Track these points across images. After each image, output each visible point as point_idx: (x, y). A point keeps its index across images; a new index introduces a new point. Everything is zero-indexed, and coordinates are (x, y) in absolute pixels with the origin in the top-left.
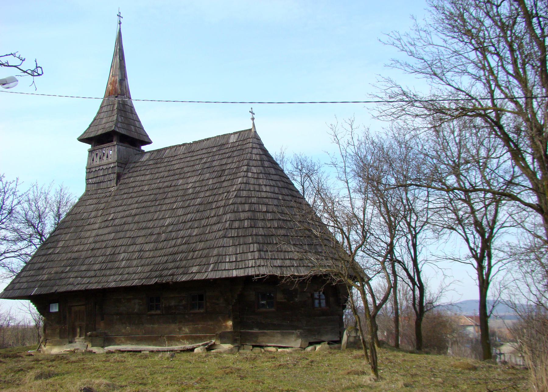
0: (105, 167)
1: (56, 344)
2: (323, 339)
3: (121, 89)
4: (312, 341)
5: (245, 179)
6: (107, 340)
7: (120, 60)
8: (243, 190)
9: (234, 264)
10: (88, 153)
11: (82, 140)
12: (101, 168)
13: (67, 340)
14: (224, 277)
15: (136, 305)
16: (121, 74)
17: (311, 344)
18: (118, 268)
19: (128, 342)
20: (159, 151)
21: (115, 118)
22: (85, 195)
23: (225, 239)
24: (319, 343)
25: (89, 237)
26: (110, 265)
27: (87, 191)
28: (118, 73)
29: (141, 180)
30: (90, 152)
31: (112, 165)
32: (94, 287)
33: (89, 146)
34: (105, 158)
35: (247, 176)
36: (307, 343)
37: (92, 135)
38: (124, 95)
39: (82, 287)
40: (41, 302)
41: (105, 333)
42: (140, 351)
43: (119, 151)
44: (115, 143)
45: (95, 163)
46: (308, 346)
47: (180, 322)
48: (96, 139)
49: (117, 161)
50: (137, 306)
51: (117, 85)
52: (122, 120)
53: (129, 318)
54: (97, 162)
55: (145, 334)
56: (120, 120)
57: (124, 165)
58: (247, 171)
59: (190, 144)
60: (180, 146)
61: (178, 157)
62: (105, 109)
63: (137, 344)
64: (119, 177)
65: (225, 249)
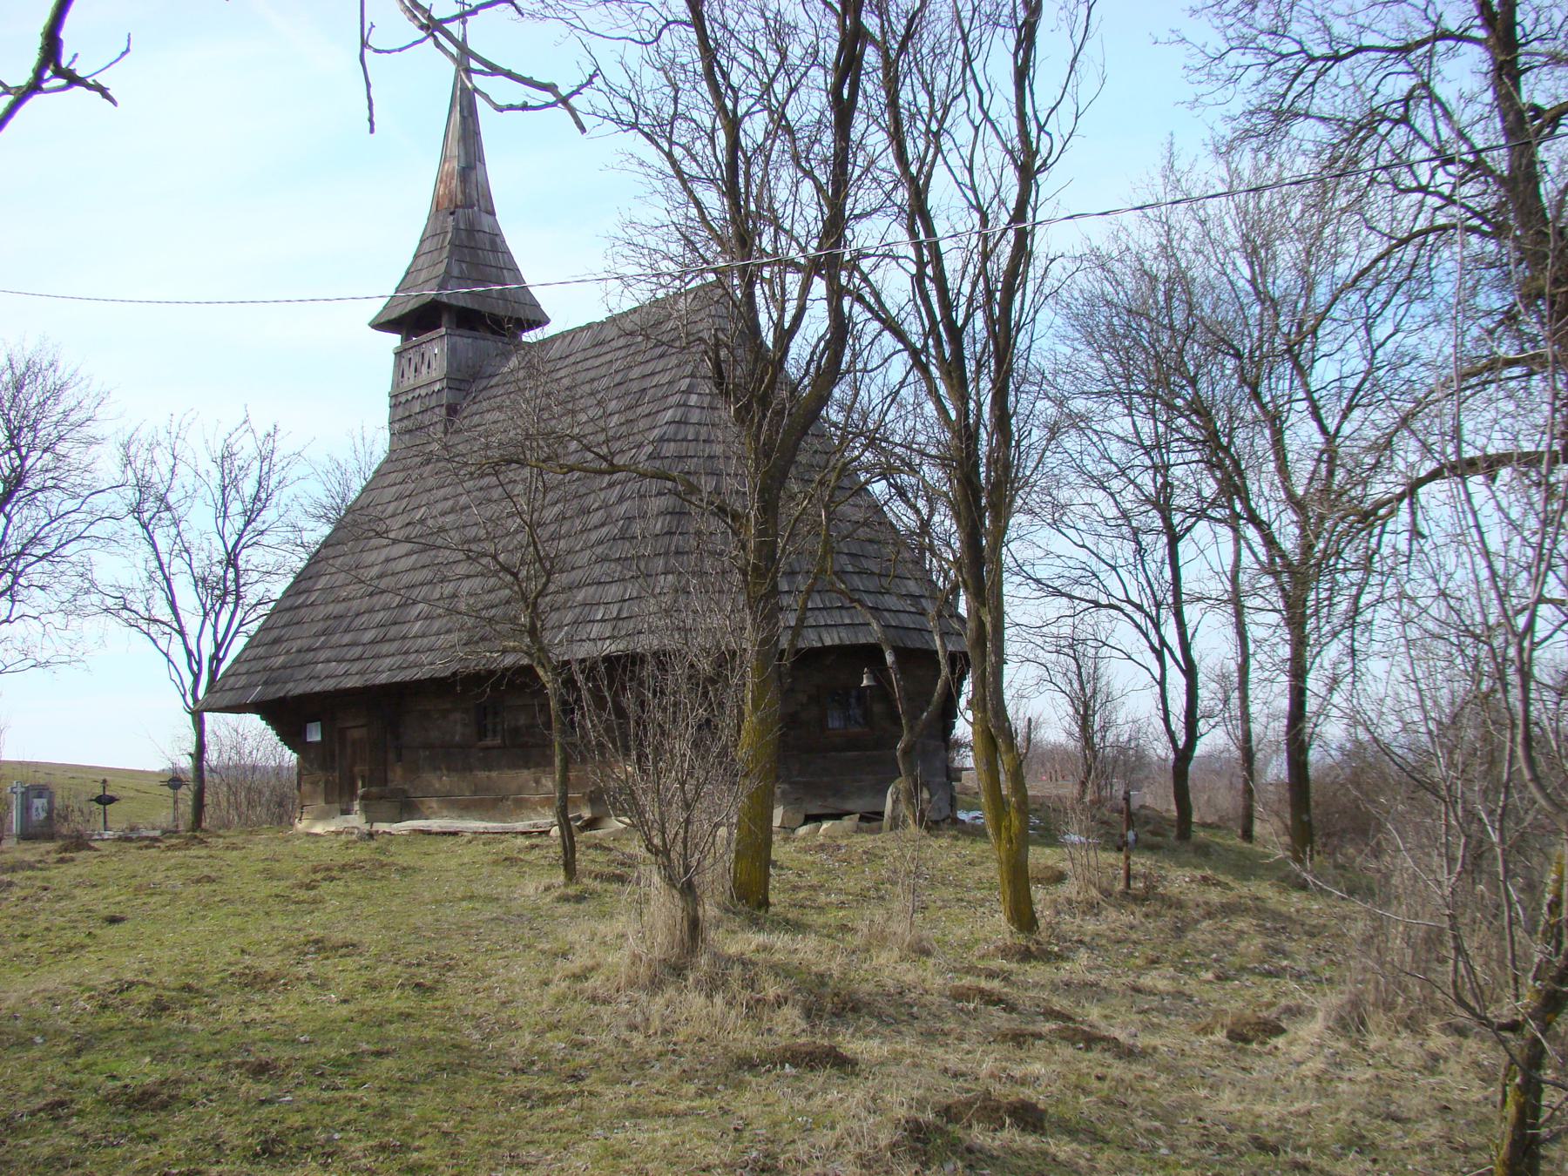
0: (423, 392)
1: (323, 816)
2: (849, 806)
3: (463, 192)
4: (816, 812)
5: (680, 411)
6: (407, 808)
7: (463, 118)
8: (669, 440)
9: (609, 626)
10: (393, 356)
11: (382, 325)
12: (416, 394)
13: (337, 806)
14: (1006, 608)
15: (457, 726)
16: (467, 154)
17: (809, 819)
18: (404, 638)
19: (445, 813)
20: (563, 335)
21: (442, 268)
22: (388, 461)
23: (606, 565)
24: (838, 816)
25: (372, 565)
26: (393, 631)
27: (392, 451)
28: (454, 149)
29: (497, 419)
30: (399, 354)
31: (437, 387)
32: (350, 683)
33: (395, 340)
34: (424, 369)
35: (685, 405)
36: (801, 818)
37: (394, 315)
38: (472, 207)
39: (330, 685)
40: (286, 716)
41: (404, 791)
42: (455, 834)
43: (453, 351)
44: (443, 330)
45: (406, 383)
46: (805, 823)
47: (537, 765)
48: (410, 321)
49: (448, 377)
50: (459, 728)
51: (455, 182)
52: (461, 271)
53: (454, 757)
54: (410, 380)
55: (475, 793)
56: (456, 272)
57: (464, 381)
58: (689, 391)
59: (602, 323)
60: (582, 329)
61: (572, 359)
62: (427, 247)
63: (461, 817)
64: (452, 410)
65: (601, 588)
